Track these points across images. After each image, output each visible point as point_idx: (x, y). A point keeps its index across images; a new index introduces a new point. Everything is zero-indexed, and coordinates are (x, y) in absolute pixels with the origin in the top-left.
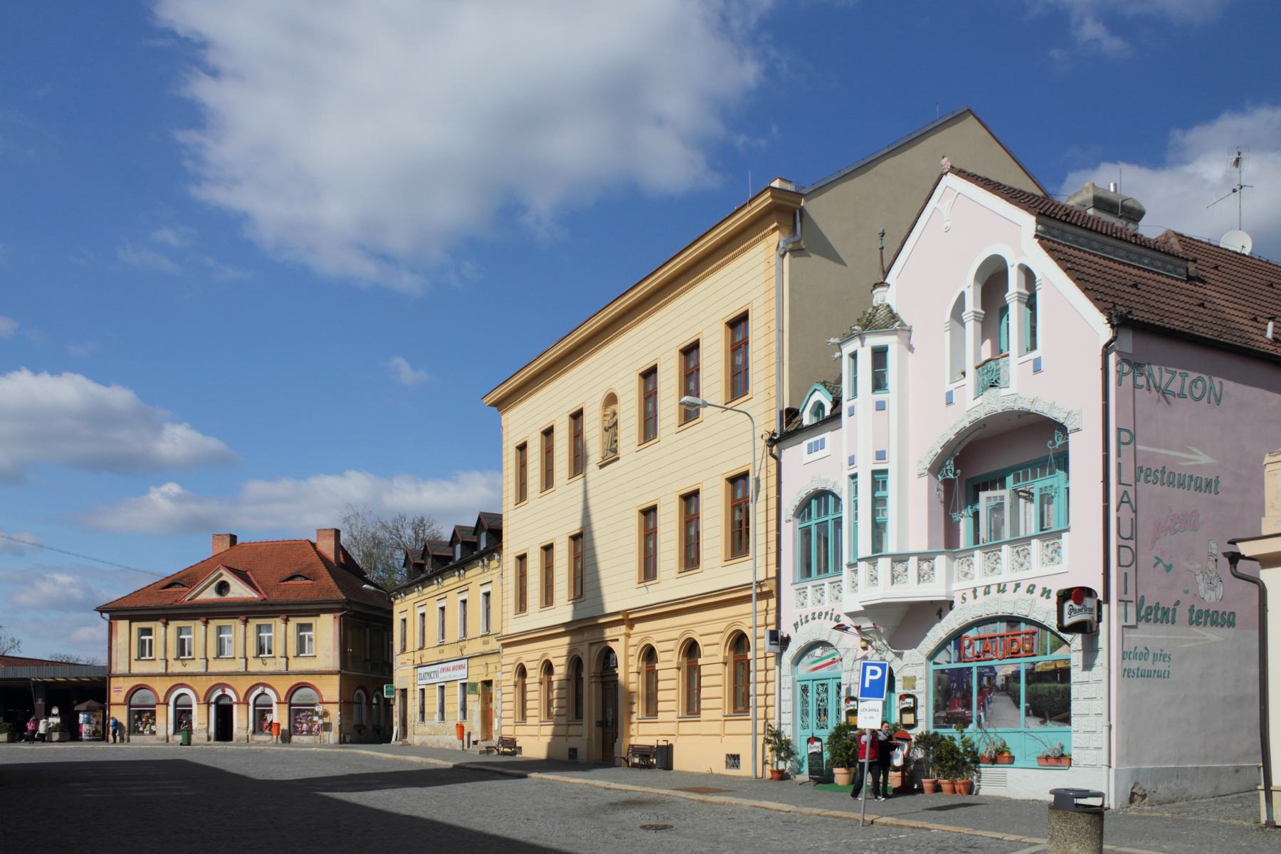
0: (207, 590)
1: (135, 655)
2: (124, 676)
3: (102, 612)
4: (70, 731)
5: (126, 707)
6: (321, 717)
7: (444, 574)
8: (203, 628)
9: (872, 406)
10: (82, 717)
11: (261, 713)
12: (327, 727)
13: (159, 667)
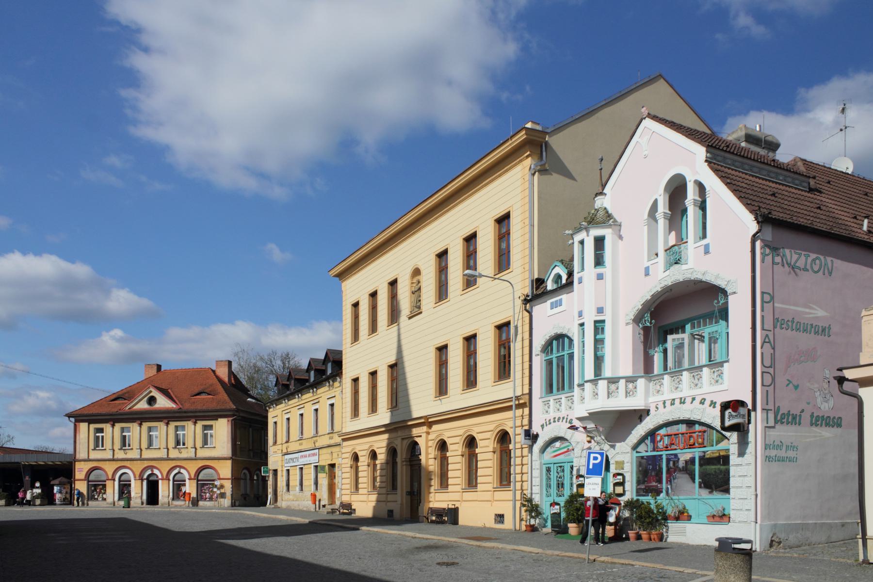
0: (141, 402)
1: (92, 446)
2: (84, 460)
3: (69, 417)
4: (48, 498)
5: (86, 482)
6: (219, 489)
7: (303, 391)
8: (138, 428)
9: (594, 277)
10: (56, 489)
11: (178, 486)
12: (223, 495)
13: (108, 455)
